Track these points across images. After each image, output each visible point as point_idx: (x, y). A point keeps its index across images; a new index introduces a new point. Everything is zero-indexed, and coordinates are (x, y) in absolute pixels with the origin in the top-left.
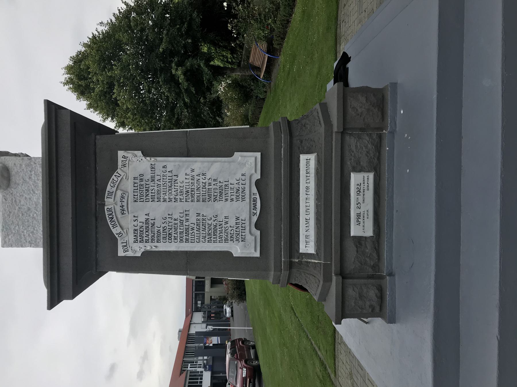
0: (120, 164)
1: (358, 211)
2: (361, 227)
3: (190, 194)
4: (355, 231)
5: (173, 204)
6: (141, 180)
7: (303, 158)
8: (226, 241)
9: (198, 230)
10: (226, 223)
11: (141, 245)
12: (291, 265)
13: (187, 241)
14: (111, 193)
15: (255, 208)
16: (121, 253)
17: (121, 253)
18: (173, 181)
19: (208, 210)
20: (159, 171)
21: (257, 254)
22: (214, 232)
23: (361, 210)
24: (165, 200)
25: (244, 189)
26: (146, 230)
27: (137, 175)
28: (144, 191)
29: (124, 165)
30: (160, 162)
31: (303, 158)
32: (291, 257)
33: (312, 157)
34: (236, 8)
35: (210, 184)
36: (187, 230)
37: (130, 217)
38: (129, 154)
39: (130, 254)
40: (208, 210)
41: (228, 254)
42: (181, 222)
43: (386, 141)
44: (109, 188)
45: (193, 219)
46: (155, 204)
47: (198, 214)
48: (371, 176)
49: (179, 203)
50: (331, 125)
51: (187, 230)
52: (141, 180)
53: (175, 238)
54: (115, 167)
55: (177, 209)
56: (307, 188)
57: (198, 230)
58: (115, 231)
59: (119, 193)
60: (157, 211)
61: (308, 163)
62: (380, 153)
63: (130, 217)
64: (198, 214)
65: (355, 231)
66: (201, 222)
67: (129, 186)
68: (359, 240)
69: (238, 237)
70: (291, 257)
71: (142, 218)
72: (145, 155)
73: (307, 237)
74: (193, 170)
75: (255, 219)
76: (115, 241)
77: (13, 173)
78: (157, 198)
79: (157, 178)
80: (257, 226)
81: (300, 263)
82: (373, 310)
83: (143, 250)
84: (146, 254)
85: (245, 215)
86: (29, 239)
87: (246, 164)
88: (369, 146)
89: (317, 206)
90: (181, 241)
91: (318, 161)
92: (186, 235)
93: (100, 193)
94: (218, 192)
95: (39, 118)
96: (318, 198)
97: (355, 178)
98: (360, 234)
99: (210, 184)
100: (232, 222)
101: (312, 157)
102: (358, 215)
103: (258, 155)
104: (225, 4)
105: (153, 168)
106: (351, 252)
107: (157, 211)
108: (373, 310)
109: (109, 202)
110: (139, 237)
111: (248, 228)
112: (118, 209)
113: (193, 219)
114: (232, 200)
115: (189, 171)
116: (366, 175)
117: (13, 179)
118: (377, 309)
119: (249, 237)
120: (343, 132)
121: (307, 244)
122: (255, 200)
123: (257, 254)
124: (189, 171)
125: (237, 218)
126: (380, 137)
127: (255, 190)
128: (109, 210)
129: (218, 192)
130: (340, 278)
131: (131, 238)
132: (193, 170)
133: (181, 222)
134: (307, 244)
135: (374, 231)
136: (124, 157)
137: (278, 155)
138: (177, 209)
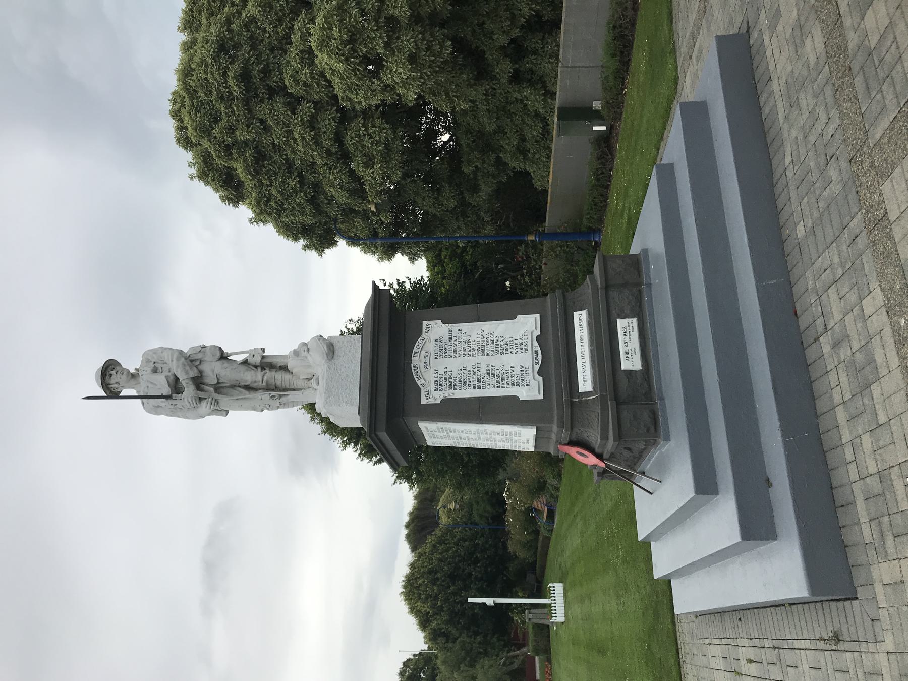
0: (424, 330)
1: (626, 349)
2: (630, 360)
3: (481, 350)
4: (625, 365)
5: (466, 358)
6: (441, 341)
7: (576, 314)
8: (513, 386)
9: (489, 378)
10: (513, 371)
11: (441, 393)
12: (572, 404)
13: (479, 387)
14: (416, 353)
15: (537, 359)
16: (424, 401)
17: (424, 401)
18: (467, 341)
19: (497, 361)
20: (455, 333)
21: (541, 397)
22: (502, 379)
23: (629, 348)
24: (460, 356)
25: (526, 343)
26: (444, 381)
27: (438, 338)
28: (443, 350)
29: (428, 331)
30: (456, 327)
31: (576, 314)
32: (571, 397)
33: (584, 313)
34: (522, 282)
35: (497, 341)
36: (479, 379)
37: (432, 371)
38: (431, 323)
39: (431, 401)
40: (497, 361)
41: (515, 398)
42: (474, 372)
43: (645, 293)
44: (415, 349)
45: (484, 369)
46: (453, 359)
47: (488, 366)
48: (635, 320)
49: (472, 357)
50: (595, 281)
51: (479, 379)
52: (441, 341)
53: (469, 386)
54: (420, 333)
55: (470, 362)
56: (581, 337)
57: (489, 378)
58: (419, 383)
59: (423, 353)
60: (454, 365)
61: (581, 319)
62: (640, 303)
63: (432, 371)
64: (488, 366)
65: (625, 365)
66: (491, 371)
67: (431, 347)
68: (629, 373)
69: (523, 382)
70: (571, 397)
71: (442, 371)
72: (444, 322)
73: (584, 377)
74: (483, 331)
75: (537, 367)
76: (419, 391)
77: (336, 348)
78: (453, 354)
79: (454, 339)
80: (539, 373)
81: (580, 401)
82: (648, 431)
83: (442, 397)
84: (445, 401)
85: (528, 363)
86: (345, 400)
87: (527, 325)
88: (630, 297)
89: (591, 351)
90: (474, 388)
91: (589, 314)
92: (479, 383)
93: (408, 355)
94: (506, 347)
95: (368, 293)
96: (591, 344)
97: (621, 323)
98: (631, 368)
99: (497, 341)
100: (517, 370)
101: (584, 313)
102: (627, 352)
103: (538, 316)
104: (508, 283)
105: (450, 331)
106: (624, 384)
107: (454, 365)
108: (648, 431)
109: (415, 361)
110: (439, 386)
111: (531, 374)
112: (422, 365)
113: (484, 369)
114: (517, 352)
115: (479, 332)
116: (630, 320)
117: (336, 352)
118: (652, 429)
119: (532, 382)
120: (607, 287)
121: (585, 382)
122: (536, 352)
123: (541, 397)
124: (479, 332)
125: (522, 367)
126: (640, 291)
127: (536, 344)
128: (415, 366)
129: (506, 347)
130: (615, 402)
131: (432, 387)
132: (483, 331)
133: (474, 372)
134: (585, 382)
135: (642, 366)
136: (428, 325)
137: (554, 316)
138: (470, 362)
